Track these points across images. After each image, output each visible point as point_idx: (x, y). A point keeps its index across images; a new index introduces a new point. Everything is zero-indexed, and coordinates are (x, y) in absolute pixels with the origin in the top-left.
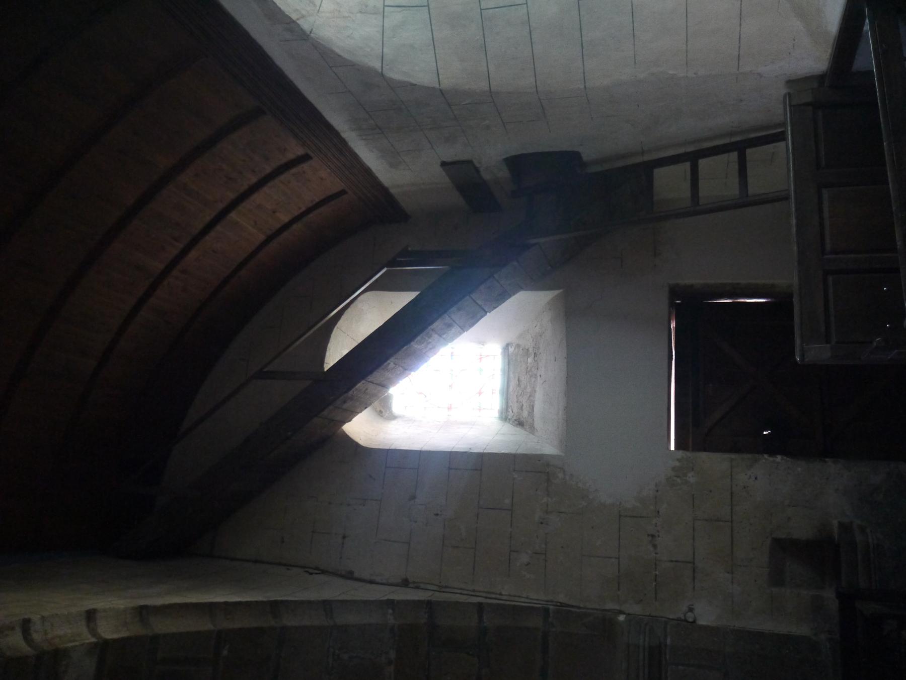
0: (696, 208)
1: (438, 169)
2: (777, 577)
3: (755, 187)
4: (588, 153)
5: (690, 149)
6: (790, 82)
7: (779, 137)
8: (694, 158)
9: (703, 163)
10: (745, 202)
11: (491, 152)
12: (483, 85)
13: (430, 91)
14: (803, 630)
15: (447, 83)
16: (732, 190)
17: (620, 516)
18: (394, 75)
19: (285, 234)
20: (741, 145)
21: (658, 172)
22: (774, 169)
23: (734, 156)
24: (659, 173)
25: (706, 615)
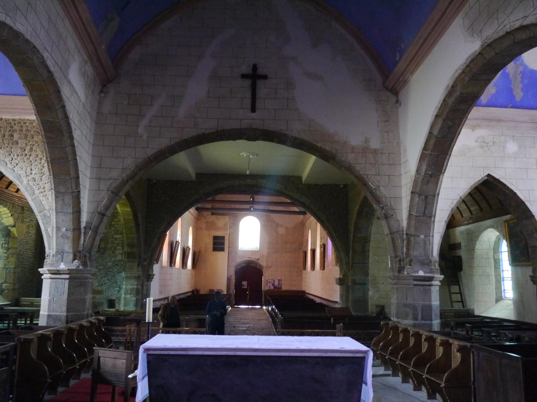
0: (450, 293)
1: (459, 242)
2: (377, 306)
3: (454, 304)
4: (462, 273)
5: (427, 41)
6: (473, 310)
7: (463, 307)
8: (460, 293)
9: (459, 295)
10: (452, 302)
11: (462, 253)
12: (475, 257)
13: (475, 247)
14: (369, 311)
15: (476, 251)
16: (454, 300)
17: (195, 118)
18: (477, 242)
19: (421, 42)
20: (462, 301)
21: (457, 287)
22: (458, 306)
23: (459, 292)
24: (457, 287)
25: (370, 293)
